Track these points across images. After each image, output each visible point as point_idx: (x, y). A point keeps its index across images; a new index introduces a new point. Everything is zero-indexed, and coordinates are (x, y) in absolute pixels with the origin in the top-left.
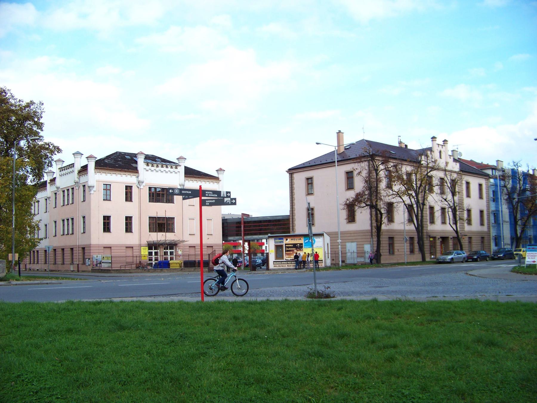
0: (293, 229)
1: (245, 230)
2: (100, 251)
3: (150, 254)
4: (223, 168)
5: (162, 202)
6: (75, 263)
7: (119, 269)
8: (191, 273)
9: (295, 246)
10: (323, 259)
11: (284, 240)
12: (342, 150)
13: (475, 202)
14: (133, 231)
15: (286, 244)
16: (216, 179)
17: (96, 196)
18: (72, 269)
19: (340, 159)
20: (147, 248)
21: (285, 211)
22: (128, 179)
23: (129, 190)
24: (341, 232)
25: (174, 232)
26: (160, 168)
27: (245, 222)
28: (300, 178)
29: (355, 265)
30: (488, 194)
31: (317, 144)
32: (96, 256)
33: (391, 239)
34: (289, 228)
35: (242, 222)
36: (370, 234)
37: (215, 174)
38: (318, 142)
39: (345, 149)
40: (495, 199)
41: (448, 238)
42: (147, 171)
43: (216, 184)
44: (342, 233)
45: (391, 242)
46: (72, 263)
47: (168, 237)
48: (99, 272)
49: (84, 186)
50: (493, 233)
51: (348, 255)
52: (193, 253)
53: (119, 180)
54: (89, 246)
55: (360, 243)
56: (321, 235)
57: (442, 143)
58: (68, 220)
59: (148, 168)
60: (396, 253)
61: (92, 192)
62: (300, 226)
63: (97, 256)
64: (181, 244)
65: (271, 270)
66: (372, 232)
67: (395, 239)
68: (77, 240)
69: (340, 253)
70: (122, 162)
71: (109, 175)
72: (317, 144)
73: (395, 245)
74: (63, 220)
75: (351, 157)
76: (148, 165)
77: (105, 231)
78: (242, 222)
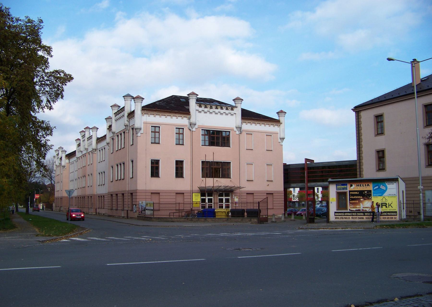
1: (308, 177)
2: (147, 197)
3: (203, 201)
4: (284, 110)
5: (214, 146)
6: (125, 209)
7: (168, 217)
8: (237, 224)
9: (361, 193)
10: (397, 210)
11: (348, 186)
14: (184, 176)
15: (350, 191)
16: (277, 122)
17: (144, 139)
18: (123, 216)
20: (199, 194)
21: (350, 155)
22: (180, 121)
23: (180, 131)
24: (422, 177)
25: (230, 178)
26: (214, 110)
27: (309, 168)
28: (368, 116)
31: (389, 59)
32: (141, 202)
34: (356, 174)
35: (306, 168)
37: (276, 117)
38: (391, 57)
42: (200, 112)
43: (276, 127)
44: (424, 178)
46: (123, 210)
47: (221, 183)
48: (144, 220)
49: (133, 129)
52: (252, 201)
53: (169, 121)
54: (136, 191)
56: (395, 180)
58: (121, 164)
59: (200, 109)
61: (139, 134)
62: (369, 170)
63: (142, 202)
64: (238, 191)
65: (332, 222)
68: (127, 187)
70: (176, 105)
71: (158, 117)
72: (389, 59)
74: (117, 165)
76: (200, 106)
77: (152, 175)
78: (306, 168)
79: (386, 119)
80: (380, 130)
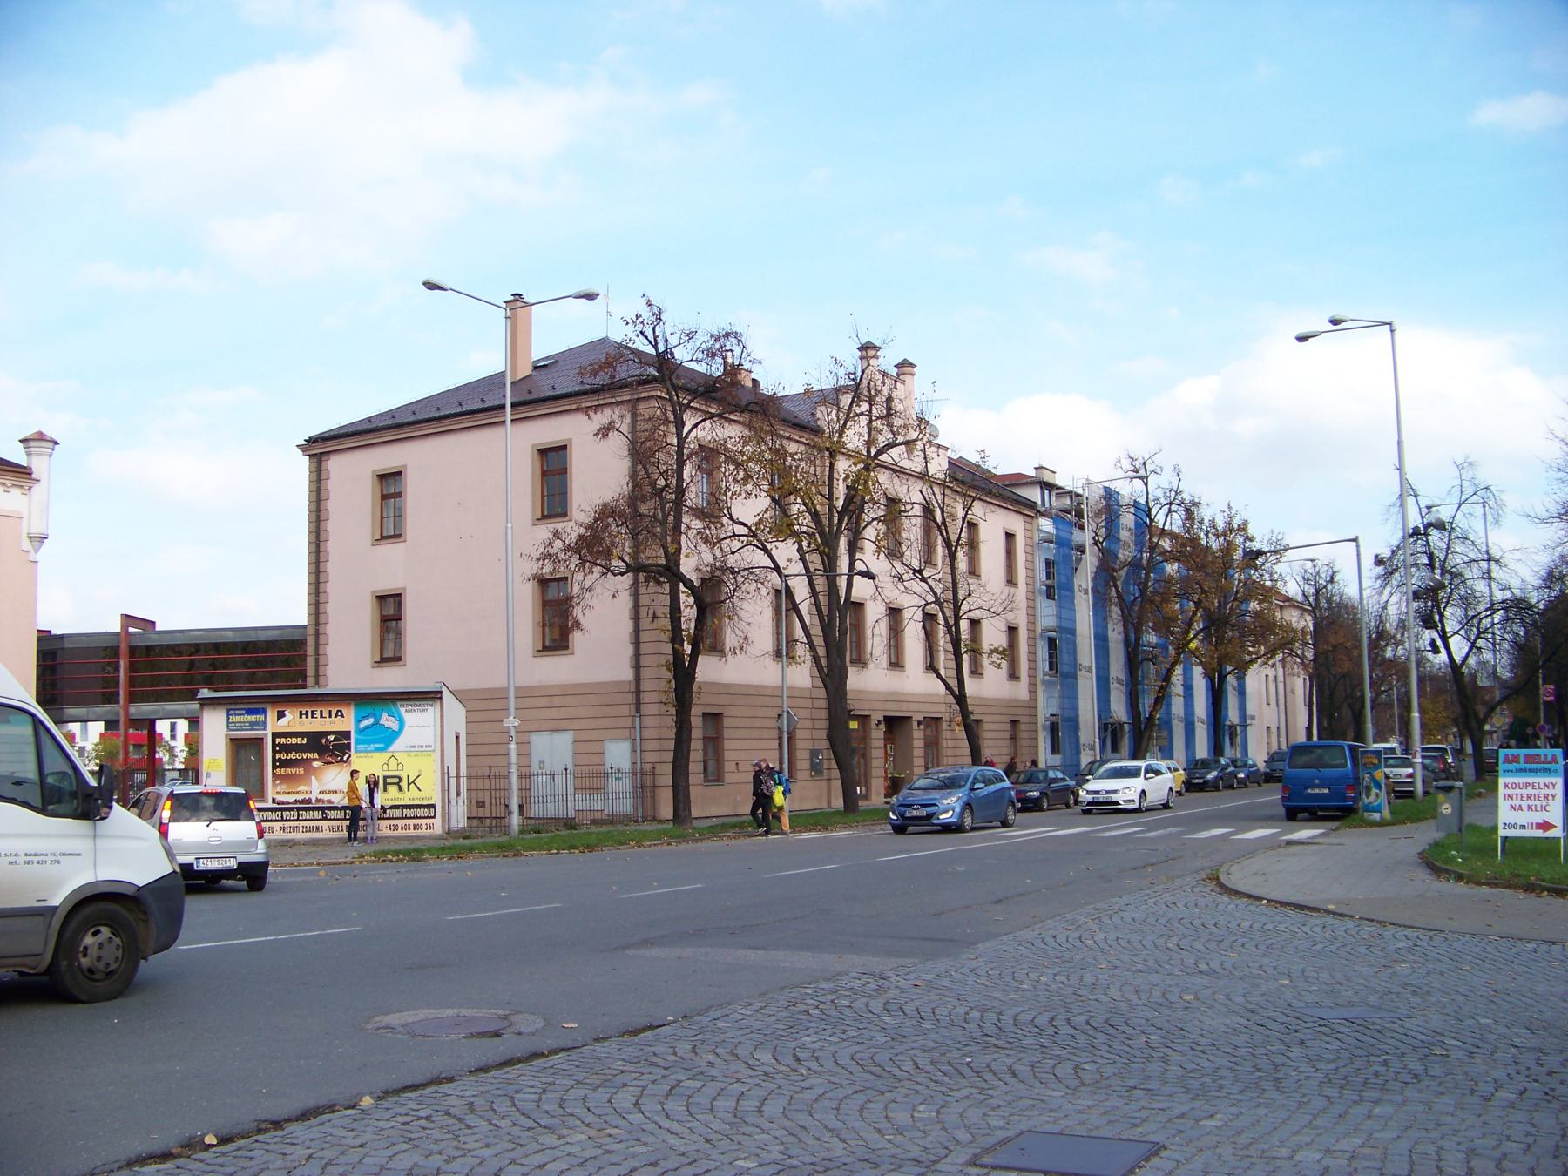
0: (317, 676)
1: (132, 682)
11: (271, 715)
12: (525, 370)
13: (999, 594)
15: (275, 735)
19: (517, 399)
21: (295, 613)
24: (517, 689)
27: (133, 650)
28: (353, 474)
29: (570, 824)
30: (1030, 569)
31: (431, 286)
33: (714, 718)
35: (123, 647)
36: (630, 698)
39: (535, 368)
40: (1056, 588)
41: (906, 720)
43: (16, 492)
44: (524, 693)
45: (711, 733)
50: (1047, 706)
51: (540, 781)
55: (594, 735)
56: (433, 696)
57: (894, 372)
60: (728, 778)
62: (348, 661)
66: (638, 692)
67: (726, 722)
69: (514, 778)
72: (431, 286)
73: (727, 744)
75: (559, 392)
78: (123, 647)
79: (412, 487)
80: (390, 530)
